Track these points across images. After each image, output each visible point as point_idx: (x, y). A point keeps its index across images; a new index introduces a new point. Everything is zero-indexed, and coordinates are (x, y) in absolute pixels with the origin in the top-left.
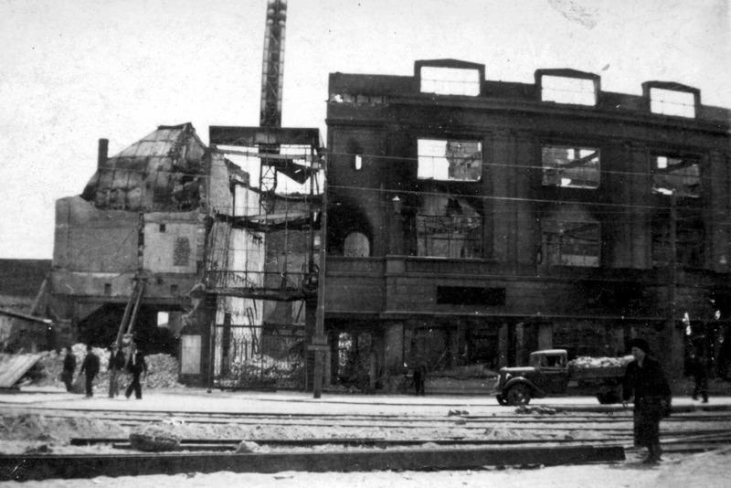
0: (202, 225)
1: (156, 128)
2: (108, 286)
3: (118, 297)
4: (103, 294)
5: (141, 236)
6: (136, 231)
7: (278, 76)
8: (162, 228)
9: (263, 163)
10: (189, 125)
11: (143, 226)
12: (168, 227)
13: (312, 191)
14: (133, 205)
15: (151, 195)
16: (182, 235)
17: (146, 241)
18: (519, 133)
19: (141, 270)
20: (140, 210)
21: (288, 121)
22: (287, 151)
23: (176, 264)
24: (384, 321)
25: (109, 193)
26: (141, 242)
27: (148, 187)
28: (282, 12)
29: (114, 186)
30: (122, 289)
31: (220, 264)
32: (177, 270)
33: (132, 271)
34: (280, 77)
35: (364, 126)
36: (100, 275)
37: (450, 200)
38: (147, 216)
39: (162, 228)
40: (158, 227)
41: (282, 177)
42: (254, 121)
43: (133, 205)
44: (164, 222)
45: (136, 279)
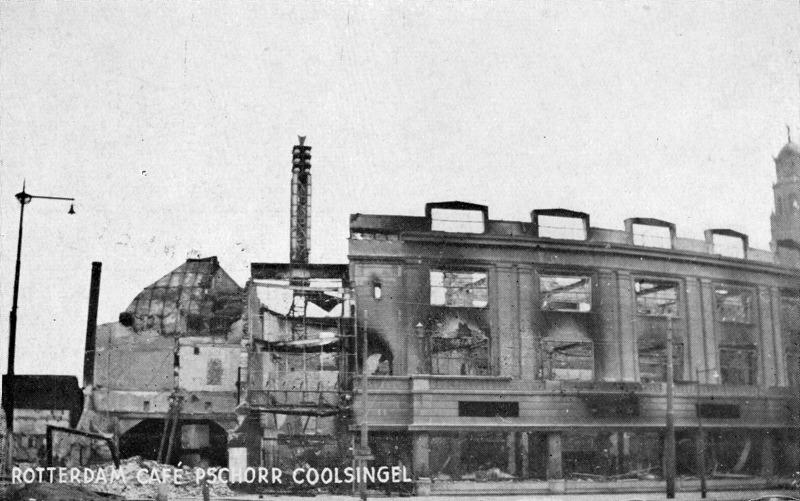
0: (245, 349)
1: (185, 261)
2: (147, 403)
3: (155, 413)
4: (142, 410)
5: (177, 358)
6: (172, 356)
7: (306, 217)
8: (197, 351)
9: (296, 294)
10: (215, 259)
11: (178, 349)
12: (201, 349)
13: (343, 313)
14: (168, 330)
15: (184, 322)
16: (214, 357)
17: (181, 362)
18: (521, 266)
19: (177, 389)
20: (175, 335)
21: (315, 258)
22: (319, 284)
23: (209, 383)
24: (412, 433)
25: (146, 318)
26: (177, 363)
27: (182, 313)
28: (307, 161)
29: (151, 314)
30: (160, 407)
31: (423, 412)
32: (211, 388)
33: (168, 390)
34: (309, 219)
35: (375, 260)
36: (139, 394)
37: (460, 325)
38: (181, 340)
39: (197, 351)
40: (192, 350)
41: (312, 306)
42: (284, 258)
43: (168, 330)
44: (198, 345)
45: (173, 397)
